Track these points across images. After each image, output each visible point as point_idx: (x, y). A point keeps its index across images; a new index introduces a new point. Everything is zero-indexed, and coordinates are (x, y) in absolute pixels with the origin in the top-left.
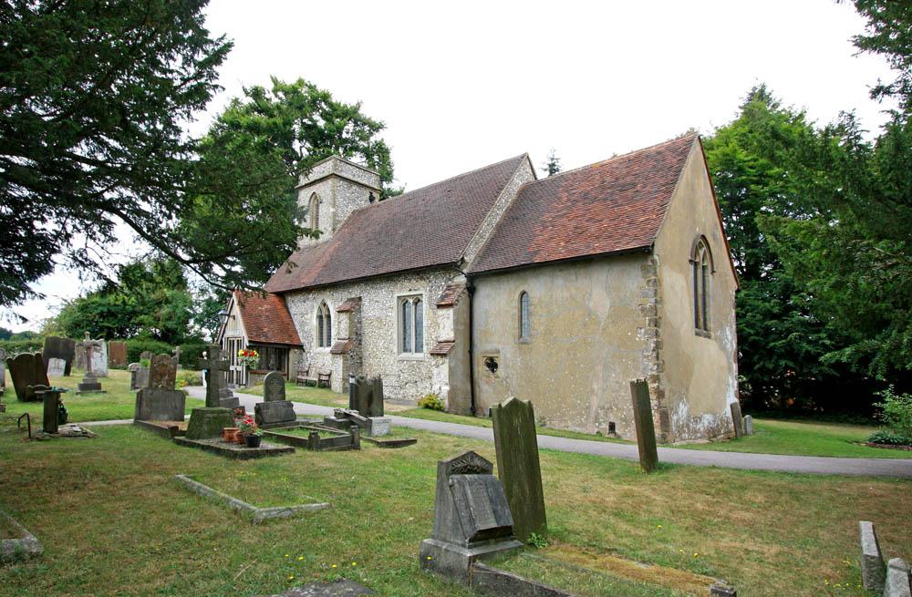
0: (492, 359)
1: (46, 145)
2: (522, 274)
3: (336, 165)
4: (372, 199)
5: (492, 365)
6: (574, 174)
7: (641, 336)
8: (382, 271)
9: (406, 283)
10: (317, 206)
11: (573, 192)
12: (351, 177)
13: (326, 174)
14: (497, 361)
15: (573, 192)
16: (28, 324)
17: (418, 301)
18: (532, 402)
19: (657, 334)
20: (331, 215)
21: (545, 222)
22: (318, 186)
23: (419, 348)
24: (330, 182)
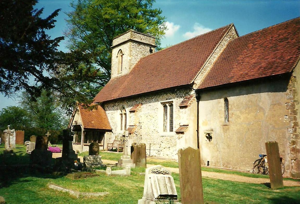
0: (209, 134)
1: (50, 55)
2: (237, 91)
3: (132, 35)
4: (151, 51)
5: (209, 137)
6: (243, 37)
7: (286, 119)
8: (153, 90)
9: (165, 96)
10: (122, 56)
11: (256, 43)
12: (139, 40)
13: (126, 40)
14: (212, 135)
15: (256, 43)
16: (116, 58)
17: (171, 105)
18: (209, 142)
19: (295, 119)
20: (128, 61)
21: (239, 60)
22: (122, 46)
23: (171, 130)
24: (129, 44)
